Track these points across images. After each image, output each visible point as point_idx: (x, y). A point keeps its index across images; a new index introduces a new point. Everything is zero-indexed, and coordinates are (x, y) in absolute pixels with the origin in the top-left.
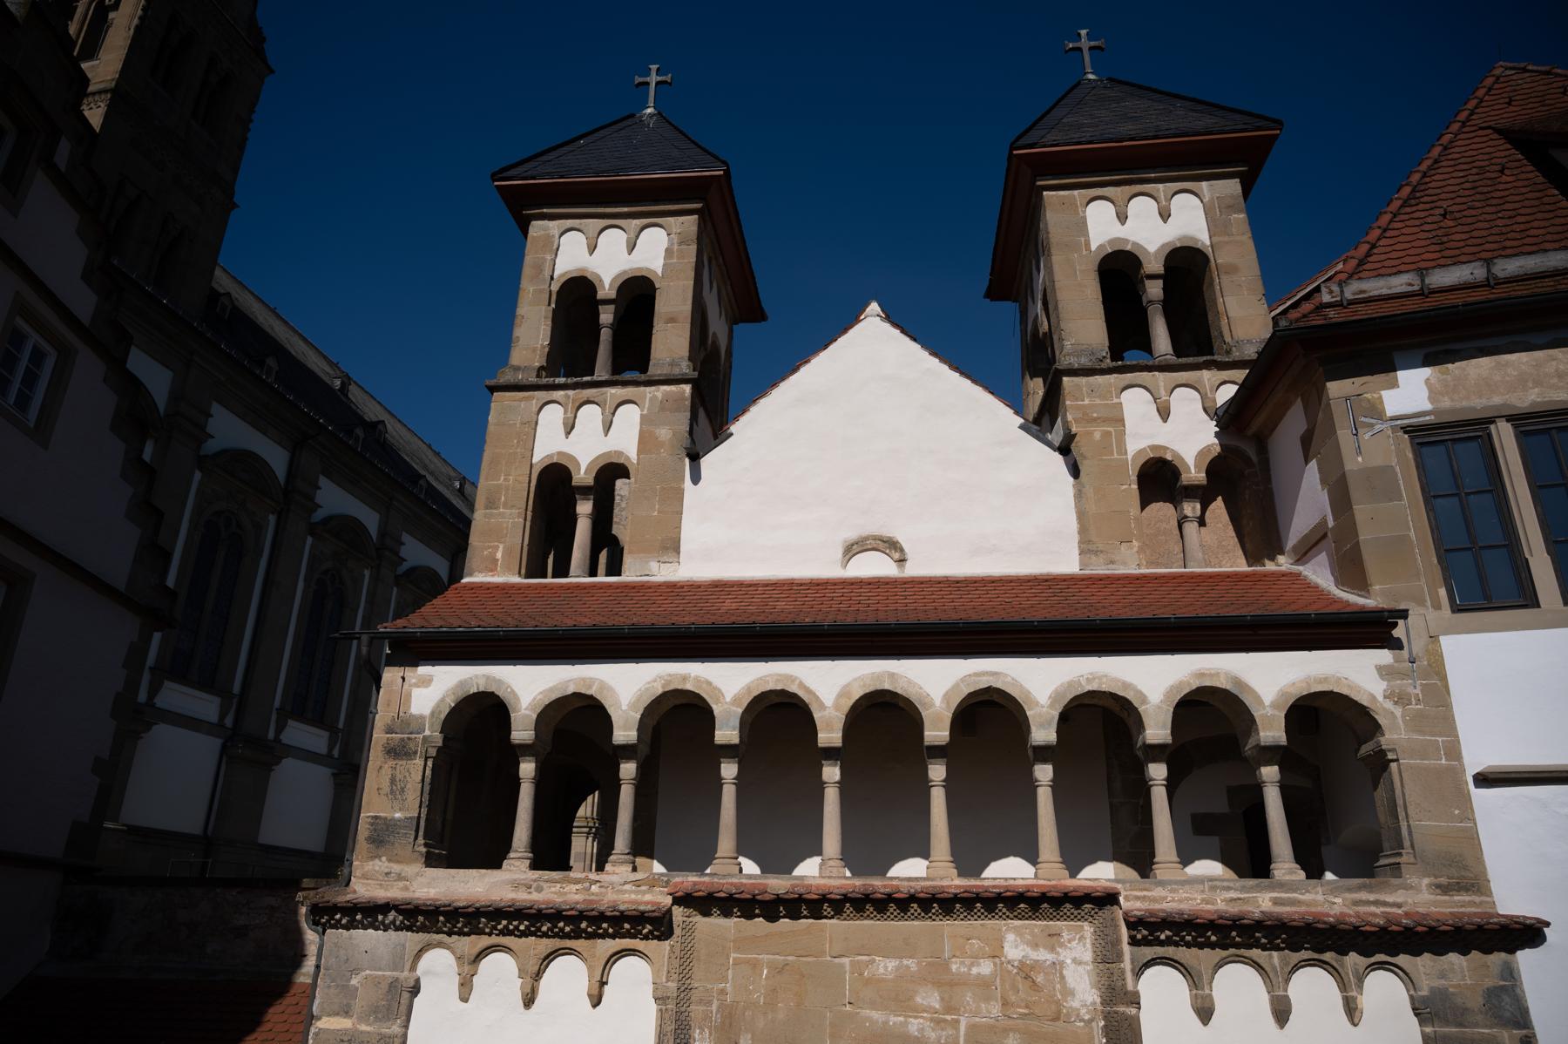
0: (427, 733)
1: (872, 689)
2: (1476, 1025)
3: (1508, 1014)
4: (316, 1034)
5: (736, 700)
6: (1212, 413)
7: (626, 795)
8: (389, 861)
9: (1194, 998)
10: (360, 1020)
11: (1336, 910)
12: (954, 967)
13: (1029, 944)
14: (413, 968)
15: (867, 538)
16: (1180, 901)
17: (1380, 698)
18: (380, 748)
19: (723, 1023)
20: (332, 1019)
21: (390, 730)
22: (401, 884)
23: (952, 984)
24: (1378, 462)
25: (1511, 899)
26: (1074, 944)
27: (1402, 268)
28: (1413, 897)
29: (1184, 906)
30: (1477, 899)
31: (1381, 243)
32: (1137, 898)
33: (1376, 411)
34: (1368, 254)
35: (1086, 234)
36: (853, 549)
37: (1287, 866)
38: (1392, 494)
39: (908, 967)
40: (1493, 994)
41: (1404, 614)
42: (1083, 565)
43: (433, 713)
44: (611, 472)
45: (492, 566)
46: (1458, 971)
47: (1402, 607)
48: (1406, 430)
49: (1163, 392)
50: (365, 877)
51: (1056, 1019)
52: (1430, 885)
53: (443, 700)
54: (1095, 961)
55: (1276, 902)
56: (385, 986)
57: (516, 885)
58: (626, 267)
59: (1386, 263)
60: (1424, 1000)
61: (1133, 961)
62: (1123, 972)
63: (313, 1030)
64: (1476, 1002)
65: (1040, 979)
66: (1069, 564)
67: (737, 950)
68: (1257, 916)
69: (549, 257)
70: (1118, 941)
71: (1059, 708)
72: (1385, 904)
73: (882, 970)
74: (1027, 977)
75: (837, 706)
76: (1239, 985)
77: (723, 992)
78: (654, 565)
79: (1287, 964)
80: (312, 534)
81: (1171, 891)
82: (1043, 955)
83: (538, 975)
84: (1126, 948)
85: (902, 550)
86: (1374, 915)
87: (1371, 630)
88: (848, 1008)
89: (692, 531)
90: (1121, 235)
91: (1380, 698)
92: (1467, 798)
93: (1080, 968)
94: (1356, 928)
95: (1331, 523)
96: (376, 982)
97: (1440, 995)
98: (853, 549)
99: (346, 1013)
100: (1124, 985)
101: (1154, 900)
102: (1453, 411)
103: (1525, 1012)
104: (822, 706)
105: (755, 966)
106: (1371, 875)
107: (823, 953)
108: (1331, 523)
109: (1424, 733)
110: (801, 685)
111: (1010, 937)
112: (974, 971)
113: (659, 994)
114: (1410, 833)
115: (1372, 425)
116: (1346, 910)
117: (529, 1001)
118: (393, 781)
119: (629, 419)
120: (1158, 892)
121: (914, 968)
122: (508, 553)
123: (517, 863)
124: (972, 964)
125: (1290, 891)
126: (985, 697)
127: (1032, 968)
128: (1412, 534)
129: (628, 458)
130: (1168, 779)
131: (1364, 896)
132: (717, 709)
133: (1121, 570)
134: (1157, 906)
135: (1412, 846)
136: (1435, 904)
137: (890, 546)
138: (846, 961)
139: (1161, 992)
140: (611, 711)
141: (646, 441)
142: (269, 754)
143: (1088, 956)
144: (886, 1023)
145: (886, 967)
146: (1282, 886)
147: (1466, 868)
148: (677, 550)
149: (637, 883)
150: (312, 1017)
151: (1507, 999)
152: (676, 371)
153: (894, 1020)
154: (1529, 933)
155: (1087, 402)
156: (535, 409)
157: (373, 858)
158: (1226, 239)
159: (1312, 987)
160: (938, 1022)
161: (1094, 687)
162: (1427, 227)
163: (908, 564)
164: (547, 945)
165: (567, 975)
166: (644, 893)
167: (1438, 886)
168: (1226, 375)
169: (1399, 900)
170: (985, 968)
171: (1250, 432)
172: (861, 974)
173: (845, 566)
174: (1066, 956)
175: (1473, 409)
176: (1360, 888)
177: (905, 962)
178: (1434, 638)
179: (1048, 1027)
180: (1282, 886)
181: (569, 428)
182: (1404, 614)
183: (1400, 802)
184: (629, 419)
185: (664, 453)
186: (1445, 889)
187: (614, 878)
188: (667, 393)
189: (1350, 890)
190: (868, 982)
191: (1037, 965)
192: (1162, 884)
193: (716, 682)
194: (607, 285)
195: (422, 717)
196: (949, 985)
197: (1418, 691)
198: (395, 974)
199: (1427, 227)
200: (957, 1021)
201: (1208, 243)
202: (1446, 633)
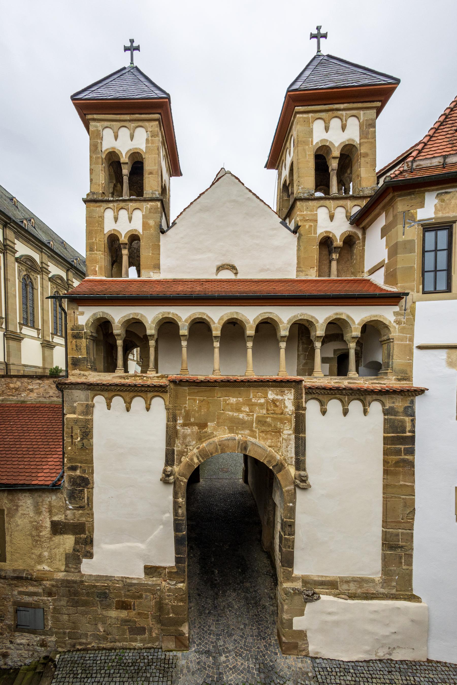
0: (85, 331)
1: (230, 317)
2: (400, 416)
3: (409, 413)
4: (66, 419)
5: (186, 321)
6: (349, 218)
7: (152, 351)
8: (80, 370)
9: (321, 409)
10: (79, 415)
11: (366, 386)
12: (253, 400)
13: (275, 394)
14: (92, 401)
15: (224, 265)
16: (321, 383)
17: (392, 322)
18: (70, 335)
19: (186, 415)
20: (70, 415)
21: (72, 330)
22: (85, 377)
23: (252, 405)
24: (410, 238)
25: (417, 383)
26: (288, 394)
27: (436, 155)
28: (390, 382)
29: (322, 384)
30: (408, 382)
31: (429, 143)
32: (308, 382)
33: (413, 218)
34: (423, 148)
35: (312, 137)
36: (220, 268)
37: (353, 373)
38: (412, 251)
39: (240, 400)
40: (406, 408)
41: (407, 294)
42: (297, 276)
43: (86, 324)
44: (134, 238)
45: (95, 274)
46: (399, 404)
47: (406, 292)
48: (422, 225)
49: (333, 209)
50: (73, 375)
51: (282, 414)
52: (395, 379)
53: (89, 320)
54: (294, 399)
55: (349, 383)
56: (84, 406)
57: (121, 377)
58: (131, 147)
59: (429, 153)
60: (387, 410)
61: (305, 399)
62: (302, 402)
63: (65, 418)
64: (401, 410)
65: (278, 404)
66: (292, 275)
67: (189, 396)
68: (344, 387)
69: (99, 141)
70: (302, 393)
71: (290, 324)
72: (381, 384)
73: (232, 401)
74: (274, 403)
75: (219, 323)
76: (334, 406)
77: (185, 407)
78: (152, 274)
79: (349, 400)
80: (17, 262)
81: (319, 380)
82: (279, 397)
83: (130, 403)
84: (304, 396)
85: (236, 269)
86: (378, 387)
87: (393, 299)
88: (222, 411)
89: (164, 261)
90: (325, 138)
91: (392, 322)
92: (411, 353)
93: (290, 401)
94: (372, 390)
95: (386, 261)
96: (82, 405)
97: (392, 408)
98: (220, 268)
99: (74, 413)
100: (302, 405)
101: (314, 382)
102: (442, 218)
103: (414, 413)
104: (214, 323)
105: (195, 400)
106: (377, 375)
107: (215, 397)
108: (386, 261)
109: (403, 333)
110: (207, 316)
111: (270, 392)
112: (259, 401)
113: (167, 408)
114: (392, 364)
115: (411, 223)
116: (369, 386)
117: (128, 410)
118: (76, 346)
119: (138, 216)
120: (315, 380)
121: (241, 401)
122: (100, 268)
123: (120, 371)
124: (258, 400)
125: (356, 379)
126: (266, 321)
127: (276, 400)
128: (416, 266)
129: (139, 232)
130: (252, 347)
131: (375, 381)
132: (180, 324)
133: (310, 278)
134: (314, 384)
135: (392, 368)
136: (395, 384)
137: (233, 268)
138: (222, 398)
139: (312, 408)
140: (145, 324)
141: (145, 225)
142: (18, 338)
143: (292, 397)
144: (233, 415)
145: (233, 400)
146: (351, 378)
147: (407, 374)
148: (159, 268)
149: (158, 377)
150: (64, 415)
151: (410, 409)
152: (154, 196)
153: (235, 414)
154: (421, 392)
155: (305, 213)
156: (103, 211)
157: (74, 369)
158: (366, 140)
159: (355, 406)
160: (248, 415)
161: (302, 317)
162: (448, 136)
163: (238, 275)
164: (132, 394)
165: (138, 403)
166: (160, 380)
167: (397, 379)
168: (356, 202)
169: (385, 383)
170: (262, 401)
171: (361, 226)
172: (226, 402)
173: (217, 275)
174: (286, 397)
175: (449, 217)
176: (374, 379)
177: (239, 399)
178: (414, 303)
179: (279, 416)
180: (351, 378)
181: (116, 219)
182: (407, 294)
183: (391, 354)
184: (138, 216)
185: (152, 231)
186: (399, 380)
187: (151, 376)
188: (151, 206)
189: (371, 379)
190: (228, 404)
191: (277, 400)
192: (316, 378)
193: (179, 314)
194: (394, 318)
195: (83, 325)
196: (252, 406)
197: (405, 320)
198: (87, 402)
199: (448, 136)
200: (253, 415)
201: (358, 142)
202: (418, 301)
